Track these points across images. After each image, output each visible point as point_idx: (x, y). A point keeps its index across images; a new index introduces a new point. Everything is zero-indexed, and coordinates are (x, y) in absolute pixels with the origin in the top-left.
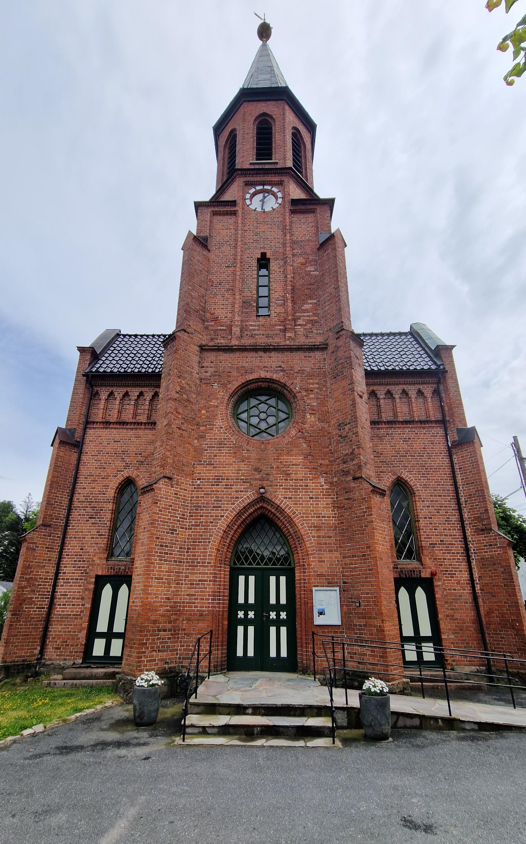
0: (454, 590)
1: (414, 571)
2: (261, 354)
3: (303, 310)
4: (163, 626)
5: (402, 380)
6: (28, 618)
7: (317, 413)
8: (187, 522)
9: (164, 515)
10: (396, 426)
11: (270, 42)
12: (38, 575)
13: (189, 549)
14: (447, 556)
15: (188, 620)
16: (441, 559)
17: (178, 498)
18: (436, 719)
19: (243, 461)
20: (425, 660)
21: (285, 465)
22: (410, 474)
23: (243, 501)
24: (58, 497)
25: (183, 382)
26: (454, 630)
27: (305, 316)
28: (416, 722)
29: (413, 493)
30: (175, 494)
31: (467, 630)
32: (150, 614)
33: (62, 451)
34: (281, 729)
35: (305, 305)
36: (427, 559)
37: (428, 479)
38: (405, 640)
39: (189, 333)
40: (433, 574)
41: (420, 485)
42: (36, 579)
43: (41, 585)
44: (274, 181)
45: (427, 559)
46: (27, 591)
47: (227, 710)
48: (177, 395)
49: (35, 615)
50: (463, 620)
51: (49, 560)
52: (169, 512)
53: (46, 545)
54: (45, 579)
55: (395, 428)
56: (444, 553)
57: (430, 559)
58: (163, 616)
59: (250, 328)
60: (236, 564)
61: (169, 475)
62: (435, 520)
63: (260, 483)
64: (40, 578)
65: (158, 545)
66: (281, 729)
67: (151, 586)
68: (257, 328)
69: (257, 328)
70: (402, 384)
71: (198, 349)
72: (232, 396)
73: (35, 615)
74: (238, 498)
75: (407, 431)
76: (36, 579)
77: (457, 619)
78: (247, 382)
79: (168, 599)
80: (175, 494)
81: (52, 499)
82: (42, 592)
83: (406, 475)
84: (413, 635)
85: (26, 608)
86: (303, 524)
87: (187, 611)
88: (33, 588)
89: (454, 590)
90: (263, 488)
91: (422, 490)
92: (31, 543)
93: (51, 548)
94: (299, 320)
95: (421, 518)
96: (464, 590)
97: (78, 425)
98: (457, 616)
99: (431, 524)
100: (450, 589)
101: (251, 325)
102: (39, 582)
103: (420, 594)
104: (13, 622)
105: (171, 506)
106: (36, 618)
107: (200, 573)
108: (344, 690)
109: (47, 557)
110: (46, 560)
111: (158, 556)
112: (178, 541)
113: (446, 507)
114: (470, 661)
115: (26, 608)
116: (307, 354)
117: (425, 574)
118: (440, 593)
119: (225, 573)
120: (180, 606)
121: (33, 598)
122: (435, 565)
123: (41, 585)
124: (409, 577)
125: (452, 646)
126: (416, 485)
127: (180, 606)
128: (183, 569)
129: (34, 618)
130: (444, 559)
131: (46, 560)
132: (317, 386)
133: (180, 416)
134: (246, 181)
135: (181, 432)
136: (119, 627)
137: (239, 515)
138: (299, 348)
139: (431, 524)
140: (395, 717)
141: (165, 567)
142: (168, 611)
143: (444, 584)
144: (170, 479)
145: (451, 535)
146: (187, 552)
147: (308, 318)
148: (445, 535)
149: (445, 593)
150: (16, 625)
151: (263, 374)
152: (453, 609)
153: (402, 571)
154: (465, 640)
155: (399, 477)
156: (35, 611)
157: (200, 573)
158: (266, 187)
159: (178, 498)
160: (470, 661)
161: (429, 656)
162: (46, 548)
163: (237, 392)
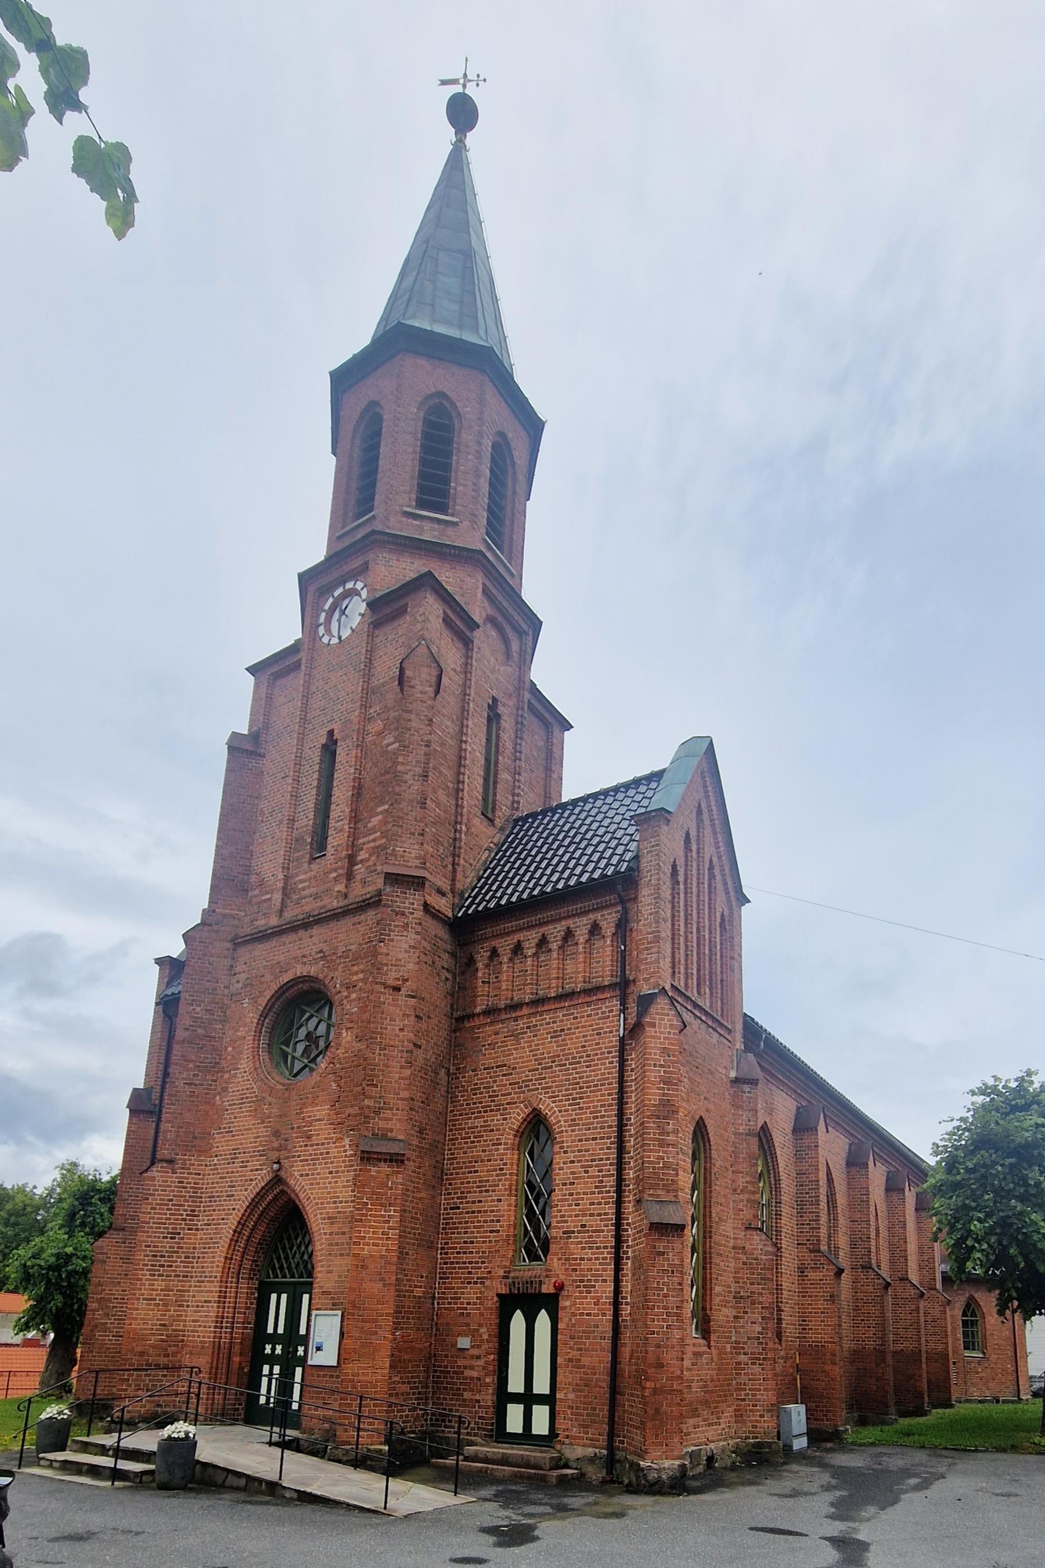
0: (588, 1314)
1: (532, 1282)
2: (301, 933)
3: (369, 830)
4: (155, 1360)
5: (563, 911)
6: (102, 1348)
7: (356, 1026)
8: (199, 1221)
9: (160, 1214)
10: (543, 1009)
11: (472, 138)
12: (112, 1294)
13: (199, 1258)
14: (587, 1254)
15: (191, 1353)
16: (576, 1259)
17: (184, 1187)
18: (260, 1481)
19: (263, 1122)
20: (534, 1432)
21: (307, 1122)
22: (553, 1102)
23: (257, 1184)
24: (132, 1188)
25: (198, 1009)
26: (577, 1385)
27: (369, 842)
28: (242, 1482)
29: (550, 1137)
30: (179, 1182)
31: (596, 1386)
32: (134, 1344)
33: (135, 1124)
34: (101, 1469)
35: (373, 820)
36: (555, 1260)
37: (581, 1108)
38: (548, 1400)
39: (210, 925)
40: (560, 1287)
41: (565, 1121)
42: (110, 1300)
43: (116, 1307)
44: (356, 568)
45: (555, 1260)
46: (98, 1315)
47: (95, 1450)
48: (187, 1033)
49: (111, 1344)
50: (594, 1368)
51: (125, 1275)
52: (168, 1209)
53: (119, 1254)
54: (121, 1299)
55: (541, 1014)
56: (583, 1248)
57: (559, 1259)
58: (154, 1347)
59: (300, 886)
60: (269, 1277)
61: (168, 1157)
62: (579, 1188)
63: (277, 1154)
64: (115, 1299)
65: (148, 1256)
66: (101, 1469)
67: (137, 1309)
68: (307, 884)
69: (307, 884)
70: (565, 918)
71: (229, 945)
72: (264, 1015)
73: (111, 1344)
74: (251, 1180)
75: (559, 1018)
76: (110, 1300)
77: (584, 1367)
78: (281, 987)
79: (164, 1325)
80: (179, 1182)
81: (125, 1192)
82: (119, 1316)
83: (547, 1107)
84: (522, 1391)
85: (99, 1336)
86: (316, 1215)
87: (191, 1341)
88: (106, 1311)
89: (588, 1314)
90: (278, 1162)
91: (567, 1131)
92: (100, 1253)
93: (127, 1259)
94: (361, 853)
95: (558, 1185)
96: (604, 1315)
97: (156, 1081)
98: (585, 1361)
99: (571, 1194)
100: (582, 1314)
101: (302, 881)
102: (113, 1303)
103: (543, 1320)
104: (85, 1352)
105: (172, 1200)
106: (113, 1348)
107: (207, 1292)
108: (280, 1450)
109: (122, 1271)
110: (121, 1274)
111: (148, 1270)
112: (182, 1248)
113: (601, 1159)
114: (591, 1440)
115: (99, 1336)
116: (356, 919)
117: (547, 1288)
118: (566, 1320)
119: (244, 1291)
120: (184, 1336)
121: (107, 1323)
122: (566, 1270)
123: (116, 1307)
124: (523, 1293)
125: (569, 1412)
126: (560, 1121)
127: (184, 1336)
128: (190, 1286)
129: (110, 1348)
130: (582, 1259)
131: (121, 1274)
132: (361, 976)
133: (191, 1065)
134: (319, 589)
135: (192, 1088)
136: (541, 1386)
137: (253, 1204)
138: (345, 911)
139: (571, 1194)
140: (225, 1474)
141: (159, 1284)
142: (162, 1341)
143: (574, 1304)
144: (171, 1162)
145: (599, 1215)
146: (197, 1263)
147: (373, 844)
148: (592, 1215)
149: (573, 1321)
150: (88, 1356)
151: (300, 970)
152: (580, 1349)
153: (514, 1283)
154: (590, 1403)
155: (535, 1109)
156: (111, 1340)
157: (207, 1292)
158: (336, 594)
159: (184, 1187)
160: (591, 1440)
161: (541, 1425)
162: (121, 1259)
163: (272, 1007)
